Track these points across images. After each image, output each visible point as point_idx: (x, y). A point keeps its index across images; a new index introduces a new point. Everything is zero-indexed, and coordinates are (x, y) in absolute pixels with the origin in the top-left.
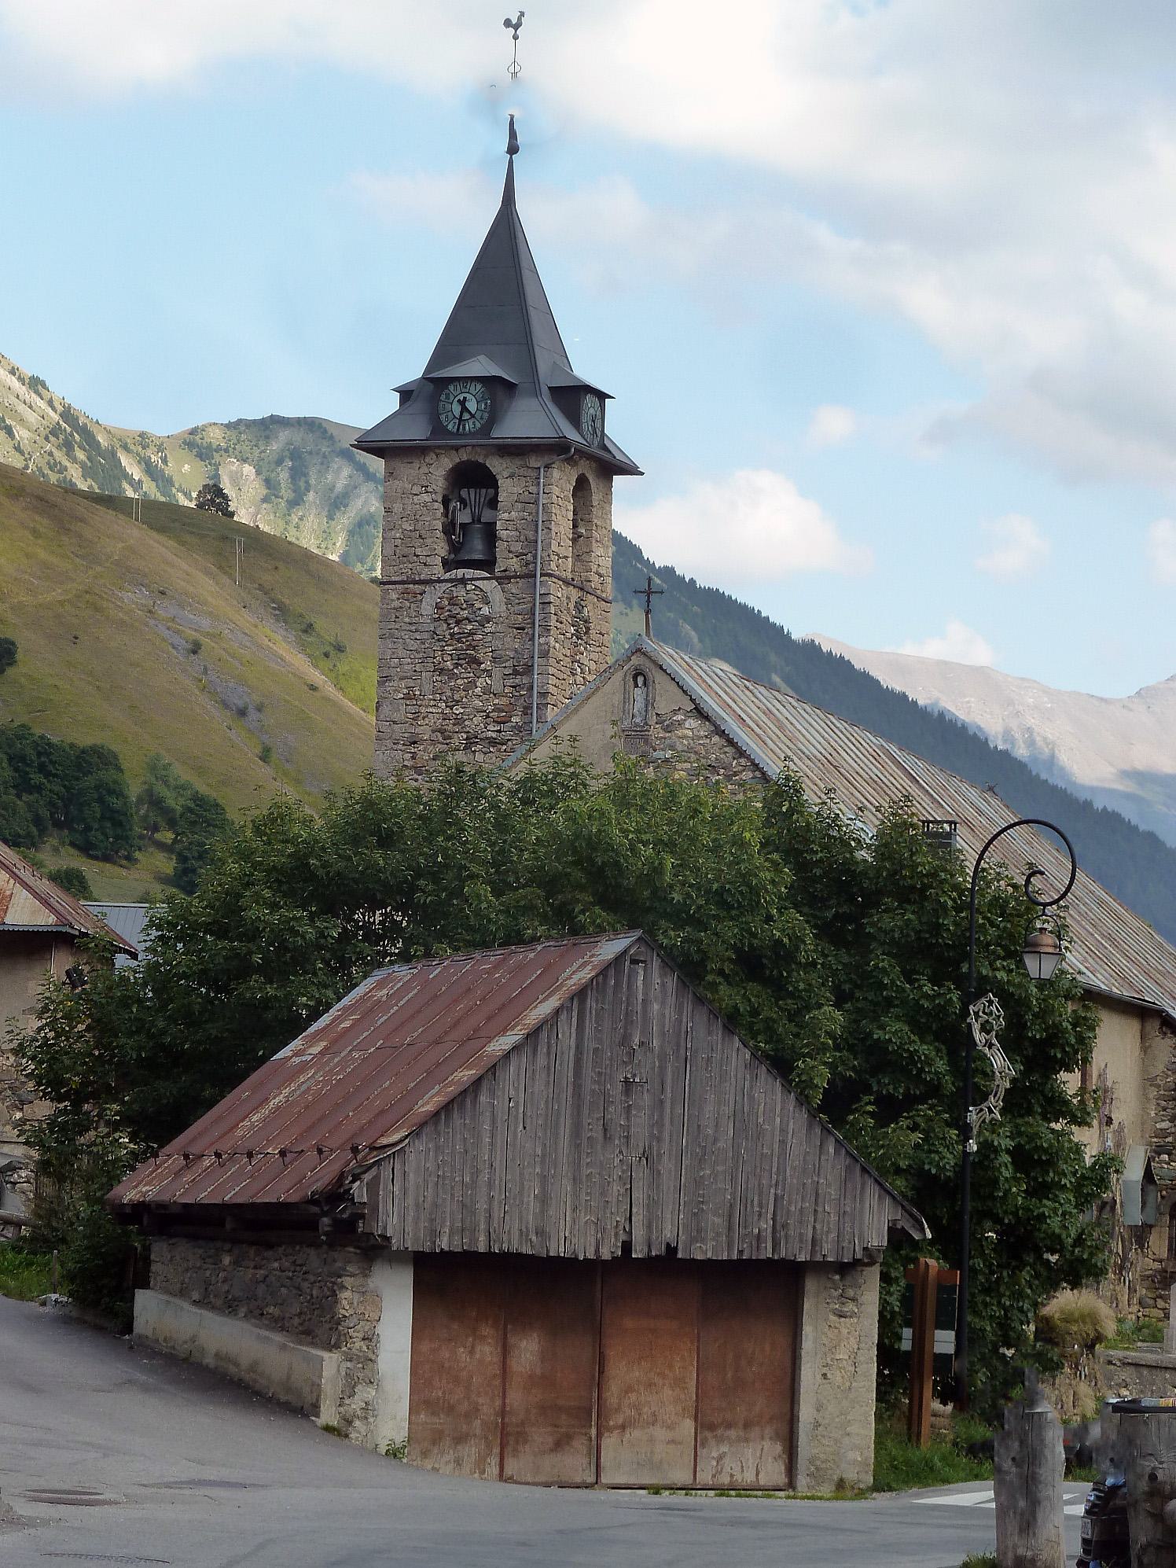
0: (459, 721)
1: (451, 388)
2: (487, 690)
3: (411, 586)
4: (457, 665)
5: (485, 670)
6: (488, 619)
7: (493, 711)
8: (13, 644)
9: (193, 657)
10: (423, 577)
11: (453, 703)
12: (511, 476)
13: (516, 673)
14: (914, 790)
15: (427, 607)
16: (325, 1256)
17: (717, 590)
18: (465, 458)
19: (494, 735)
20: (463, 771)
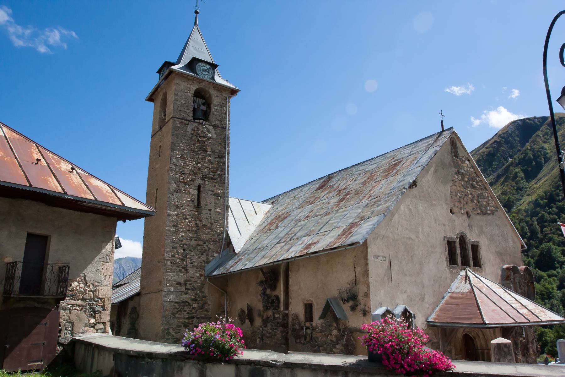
0: (199, 169)
1: (200, 63)
2: (209, 161)
3: (184, 121)
4: (199, 151)
5: (208, 154)
6: (210, 138)
7: (211, 168)
8: (478, 243)
9: (442, 253)
10: (188, 119)
11: (198, 163)
12: (217, 96)
13: (219, 157)
14: (41, 158)
15: (189, 129)
16: (201, 182)
17: (124, 222)
18: (202, 87)
19: (212, 176)
20: (186, 270)
